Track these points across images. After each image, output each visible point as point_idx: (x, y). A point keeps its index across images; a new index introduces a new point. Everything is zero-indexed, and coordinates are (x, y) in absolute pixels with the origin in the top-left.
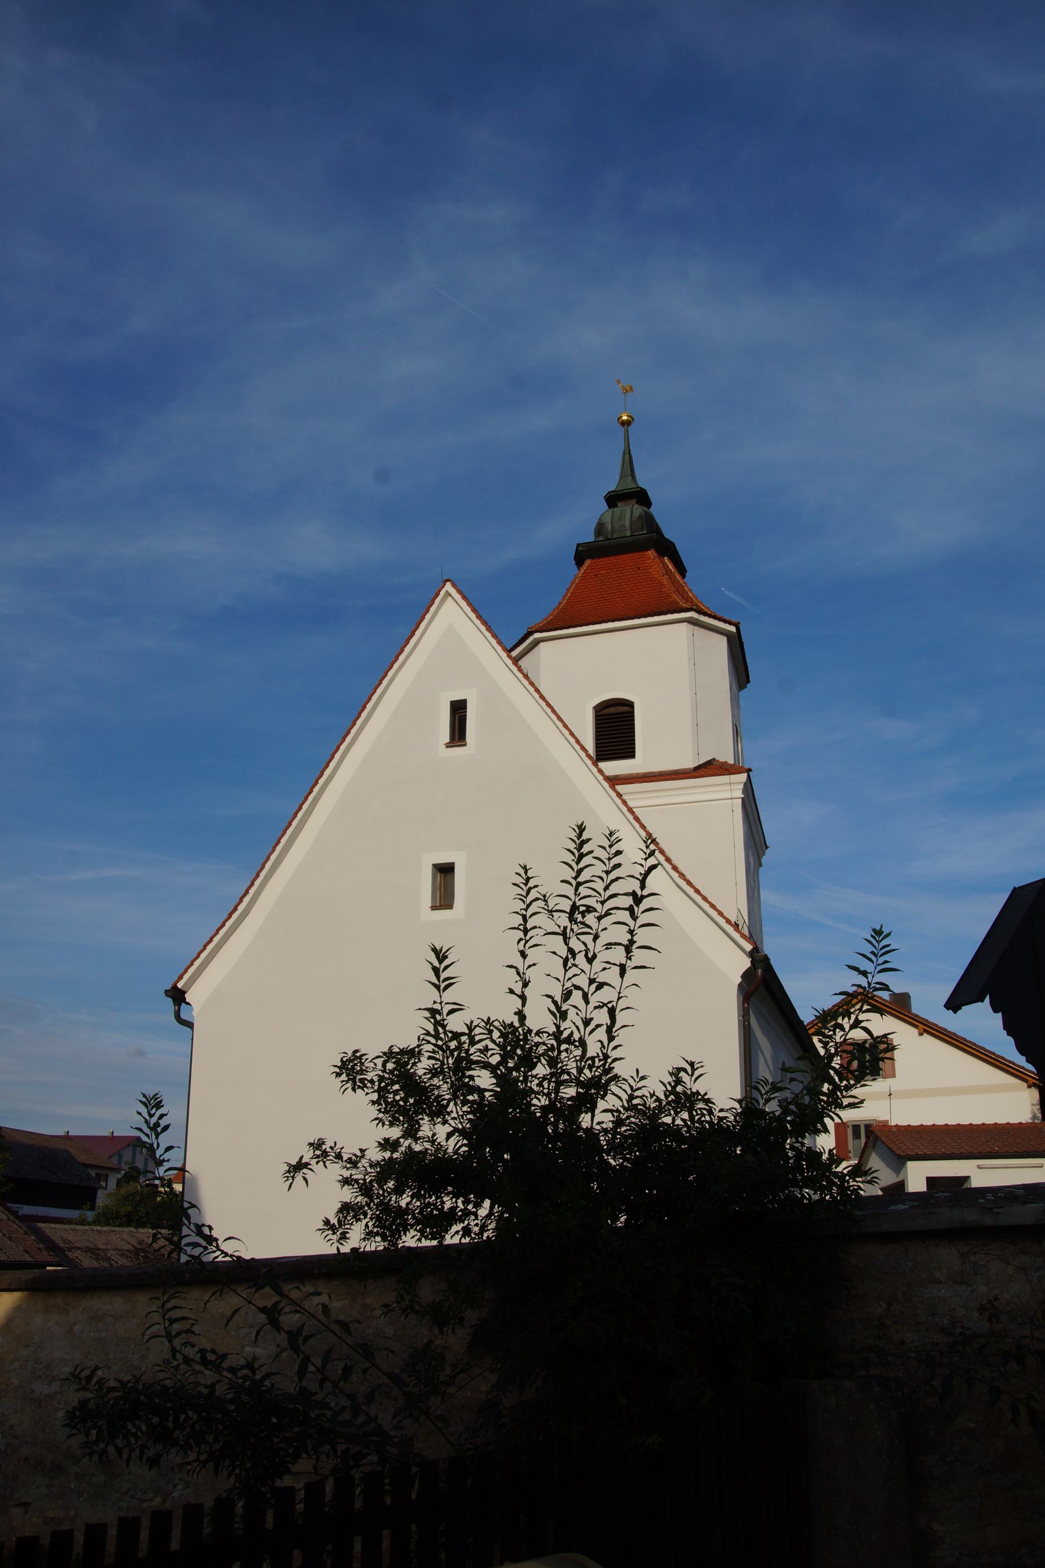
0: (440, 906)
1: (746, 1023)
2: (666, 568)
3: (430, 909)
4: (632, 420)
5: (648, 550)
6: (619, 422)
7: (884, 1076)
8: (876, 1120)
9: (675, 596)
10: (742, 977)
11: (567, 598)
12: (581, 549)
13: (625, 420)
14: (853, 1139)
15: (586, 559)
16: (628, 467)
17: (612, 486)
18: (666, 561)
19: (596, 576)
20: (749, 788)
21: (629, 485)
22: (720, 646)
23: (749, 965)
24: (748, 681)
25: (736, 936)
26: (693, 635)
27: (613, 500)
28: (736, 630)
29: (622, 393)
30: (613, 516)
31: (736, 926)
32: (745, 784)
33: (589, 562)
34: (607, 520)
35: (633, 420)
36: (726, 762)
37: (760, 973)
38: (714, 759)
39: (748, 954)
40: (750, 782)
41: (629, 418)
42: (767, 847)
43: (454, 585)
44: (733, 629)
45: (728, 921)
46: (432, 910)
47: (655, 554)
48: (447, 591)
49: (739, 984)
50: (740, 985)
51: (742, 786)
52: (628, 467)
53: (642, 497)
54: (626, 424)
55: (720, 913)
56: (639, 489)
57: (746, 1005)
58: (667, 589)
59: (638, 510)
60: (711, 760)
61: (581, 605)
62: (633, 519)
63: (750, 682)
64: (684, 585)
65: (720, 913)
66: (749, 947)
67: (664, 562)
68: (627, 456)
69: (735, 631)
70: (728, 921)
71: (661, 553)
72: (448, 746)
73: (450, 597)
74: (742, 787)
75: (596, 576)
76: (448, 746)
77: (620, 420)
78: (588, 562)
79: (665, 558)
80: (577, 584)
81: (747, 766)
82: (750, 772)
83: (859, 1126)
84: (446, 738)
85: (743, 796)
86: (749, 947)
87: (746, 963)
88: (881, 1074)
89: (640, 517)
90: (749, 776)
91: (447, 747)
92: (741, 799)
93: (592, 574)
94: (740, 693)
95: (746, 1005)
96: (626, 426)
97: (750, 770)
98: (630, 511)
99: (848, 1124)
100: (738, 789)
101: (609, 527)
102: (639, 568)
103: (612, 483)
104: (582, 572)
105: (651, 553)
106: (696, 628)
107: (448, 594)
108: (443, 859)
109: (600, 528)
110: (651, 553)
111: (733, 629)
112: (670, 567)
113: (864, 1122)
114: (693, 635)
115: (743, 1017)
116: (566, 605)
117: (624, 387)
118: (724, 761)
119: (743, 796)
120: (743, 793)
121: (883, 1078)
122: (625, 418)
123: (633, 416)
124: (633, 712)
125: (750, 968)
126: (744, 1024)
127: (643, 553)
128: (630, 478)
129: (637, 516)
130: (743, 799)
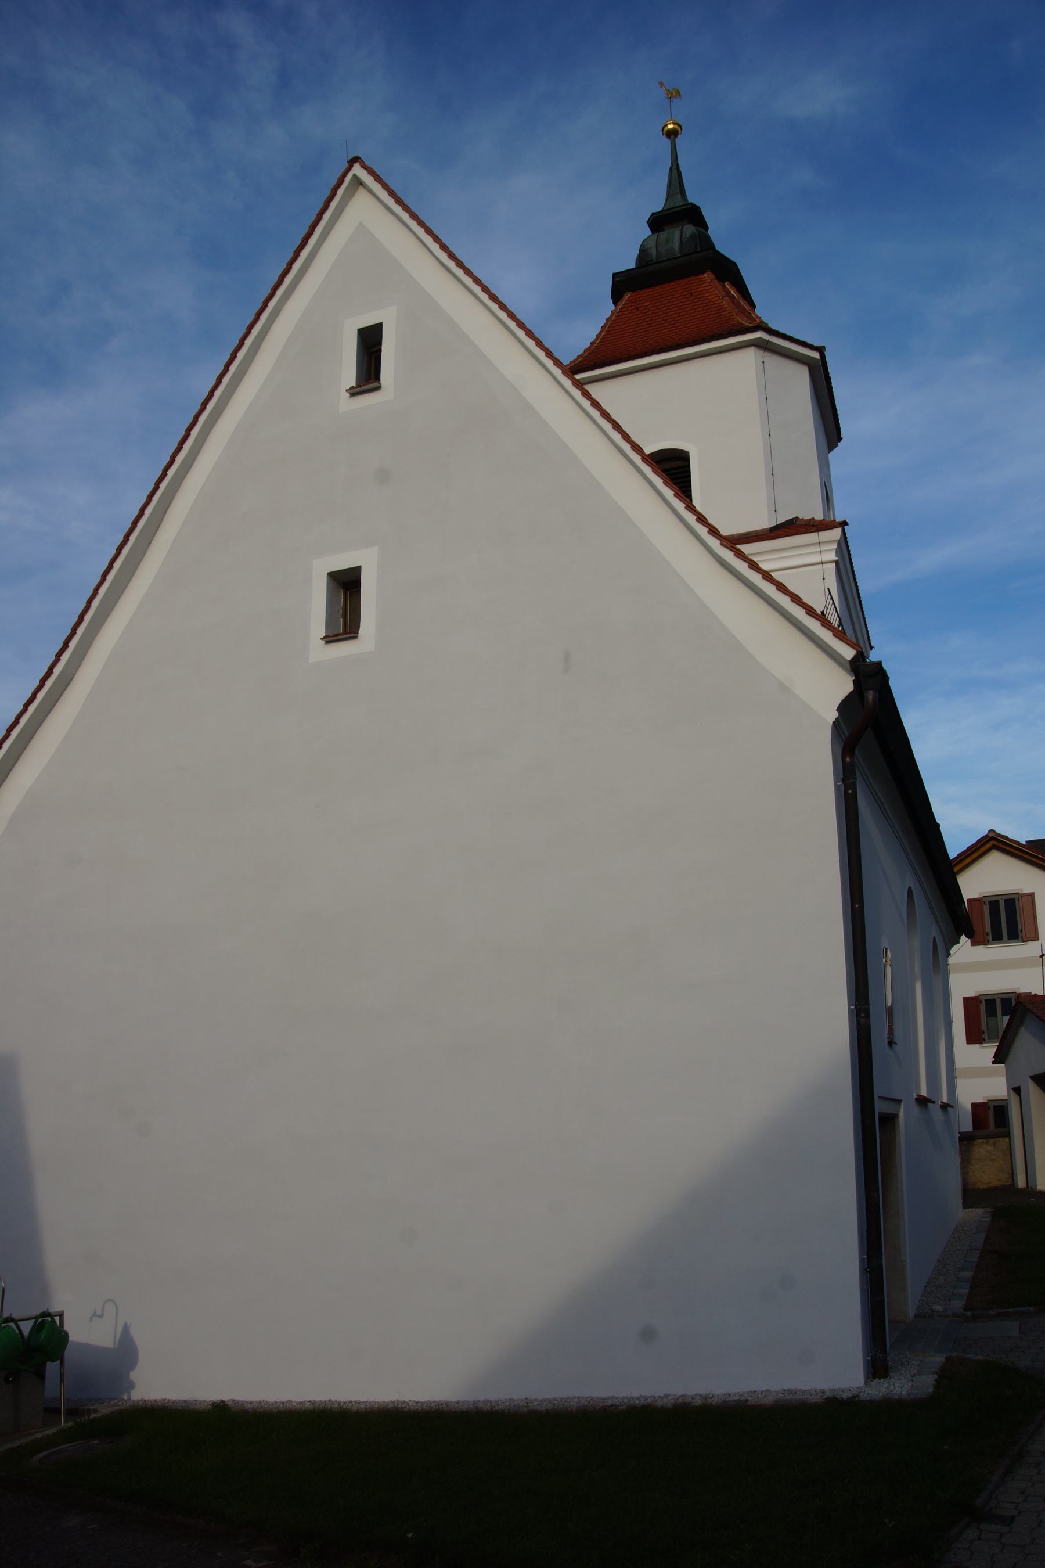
0: (345, 632)
1: (850, 791)
2: (728, 294)
3: (323, 642)
4: (679, 129)
5: (703, 273)
6: (664, 132)
7: (1024, 939)
8: (1015, 992)
9: (738, 318)
10: (840, 709)
11: (601, 337)
12: (618, 279)
13: (671, 129)
14: (987, 1016)
15: (625, 293)
16: (676, 181)
17: (658, 205)
18: (727, 286)
19: (638, 309)
20: (843, 545)
21: (678, 201)
22: (801, 376)
23: (850, 687)
24: (840, 439)
25: (826, 636)
26: (763, 362)
27: (657, 222)
28: (820, 356)
29: (667, 98)
30: (658, 241)
31: (822, 618)
32: (839, 542)
33: (629, 295)
34: (652, 244)
35: (682, 130)
36: (813, 518)
37: (871, 697)
38: (797, 517)
39: (848, 666)
40: (845, 538)
41: (676, 127)
42: (871, 648)
43: (364, 166)
44: (816, 355)
45: (810, 611)
46: (327, 642)
47: (712, 276)
48: (355, 175)
49: (834, 722)
50: (836, 724)
51: (835, 546)
52: (676, 181)
53: (693, 215)
54: (672, 134)
55: (796, 599)
56: (691, 206)
57: (848, 759)
58: (728, 312)
59: (689, 229)
60: (793, 519)
61: (619, 342)
62: (684, 240)
63: (842, 439)
64: (750, 312)
65: (796, 599)
66: (848, 653)
67: (724, 287)
68: (675, 172)
69: (819, 358)
70: (810, 611)
71: (721, 277)
72: (354, 392)
73: (361, 187)
74: (835, 547)
75: (638, 309)
76: (354, 392)
77: (666, 129)
78: (628, 296)
79: (726, 284)
80: (614, 320)
81: (839, 519)
82: (845, 527)
83: (994, 1000)
84: (350, 378)
85: (837, 558)
86: (848, 653)
87: (845, 685)
88: (1020, 937)
89: (693, 237)
90: (844, 533)
91: (353, 395)
92: (834, 564)
93: (633, 307)
94: (831, 455)
95: (848, 759)
96: (672, 137)
97: (844, 523)
98: (676, 236)
99: (981, 999)
100: (833, 549)
101: (654, 252)
102: (691, 294)
103: (658, 204)
104: (620, 307)
105: (708, 276)
106: (767, 354)
107: (358, 182)
108: (342, 562)
109: (643, 252)
110: (708, 276)
111: (816, 355)
112: (733, 292)
113: (999, 996)
114: (763, 362)
115: (843, 781)
116: (600, 344)
117: (668, 90)
118: (811, 517)
119: (837, 558)
120: (837, 555)
121: (1023, 942)
122: (671, 126)
123: (680, 123)
124: (689, 466)
125: (851, 693)
126: (846, 793)
127: (697, 277)
128: (679, 196)
129: (688, 236)
130: (837, 562)
